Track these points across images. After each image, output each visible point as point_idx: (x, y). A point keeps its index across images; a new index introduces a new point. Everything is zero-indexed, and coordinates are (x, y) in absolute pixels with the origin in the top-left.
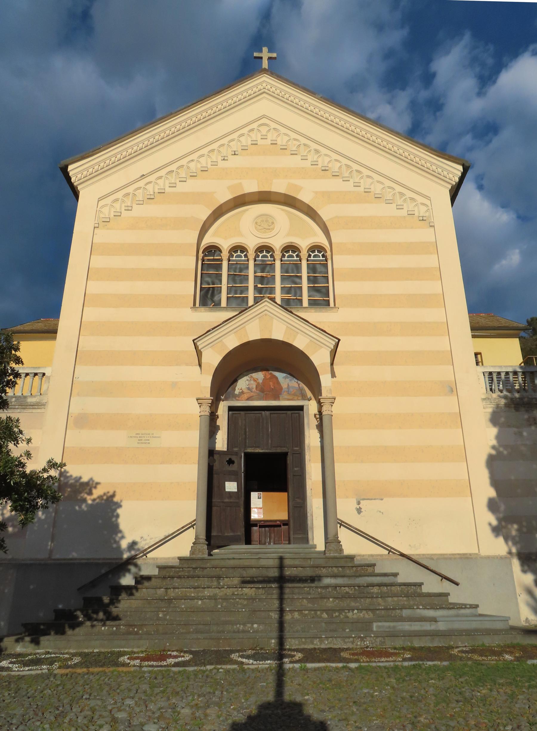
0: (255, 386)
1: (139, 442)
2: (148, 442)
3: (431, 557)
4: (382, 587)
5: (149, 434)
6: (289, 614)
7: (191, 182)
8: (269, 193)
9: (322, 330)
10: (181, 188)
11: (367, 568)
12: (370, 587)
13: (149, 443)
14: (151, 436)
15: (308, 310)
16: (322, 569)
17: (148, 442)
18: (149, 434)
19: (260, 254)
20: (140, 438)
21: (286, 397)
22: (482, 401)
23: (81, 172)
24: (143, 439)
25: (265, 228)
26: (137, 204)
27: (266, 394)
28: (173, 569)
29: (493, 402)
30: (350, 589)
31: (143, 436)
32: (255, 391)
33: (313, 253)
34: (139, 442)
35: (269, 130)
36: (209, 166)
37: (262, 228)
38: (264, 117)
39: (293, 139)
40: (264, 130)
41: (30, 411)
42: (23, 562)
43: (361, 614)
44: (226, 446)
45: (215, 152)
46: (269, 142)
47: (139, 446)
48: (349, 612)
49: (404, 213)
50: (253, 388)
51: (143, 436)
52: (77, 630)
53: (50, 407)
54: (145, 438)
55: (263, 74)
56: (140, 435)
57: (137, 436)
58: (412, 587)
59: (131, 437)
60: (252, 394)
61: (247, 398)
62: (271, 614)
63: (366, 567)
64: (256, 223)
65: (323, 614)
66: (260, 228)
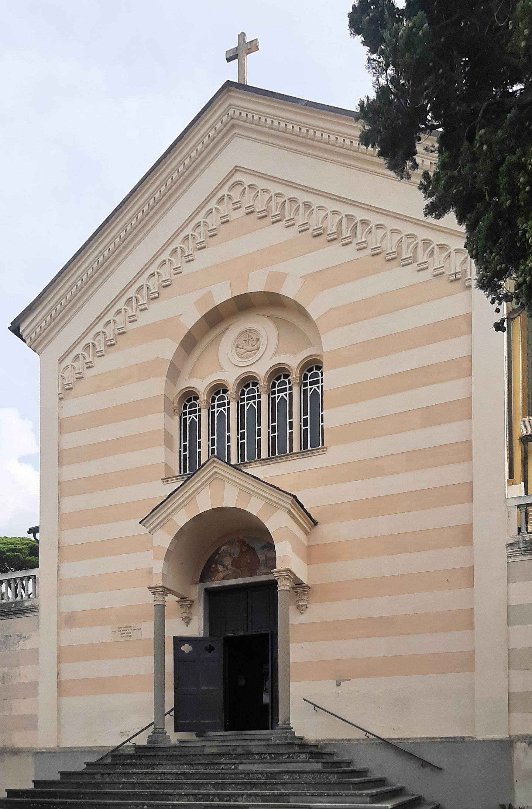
0: (230, 563)
1: (122, 635)
2: (130, 635)
3: (418, 743)
4: (293, 774)
5: (130, 627)
6: (185, 797)
7: (154, 306)
8: (245, 296)
9: (275, 487)
10: (144, 319)
11: (300, 754)
12: (282, 774)
13: (131, 636)
14: (132, 628)
15: (290, 458)
16: (255, 755)
17: (130, 635)
18: (130, 627)
19: (246, 390)
20: (123, 632)
21: (263, 571)
22: (507, 547)
23: (34, 330)
24: (125, 632)
25: (248, 351)
26: (402, 266)
27: (242, 570)
28: (123, 757)
29: (521, 546)
30: (262, 776)
31: (125, 629)
32: (231, 567)
33: (189, 403)
34: (122, 635)
35: (244, 192)
36: (173, 277)
37: (245, 351)
38: (237, 170)
39: (275, 194)
40: (236, 194)
41: (28, 615)
42: (39, 750)
43: (250, 799)
44: (202, 633)
45: (178, 251)
46: (243, 211)
47: (123, 639)
48: (238, 797)
49: (427, 275)
50: (228, 565)
51: (125, 629)
52: (503, 803)
53: (43, 610)
54: (128, 632)
55: (226, 99)
56: (123, 629)
57: (120, 629)
58: (325, 774)
59: (114, 631)
60: (228, 572)
61: (222, 577)
62: (170, 797)
63: (298, 754)
64: (237, 347)
65: (215, 798)
66: (243, 351)
